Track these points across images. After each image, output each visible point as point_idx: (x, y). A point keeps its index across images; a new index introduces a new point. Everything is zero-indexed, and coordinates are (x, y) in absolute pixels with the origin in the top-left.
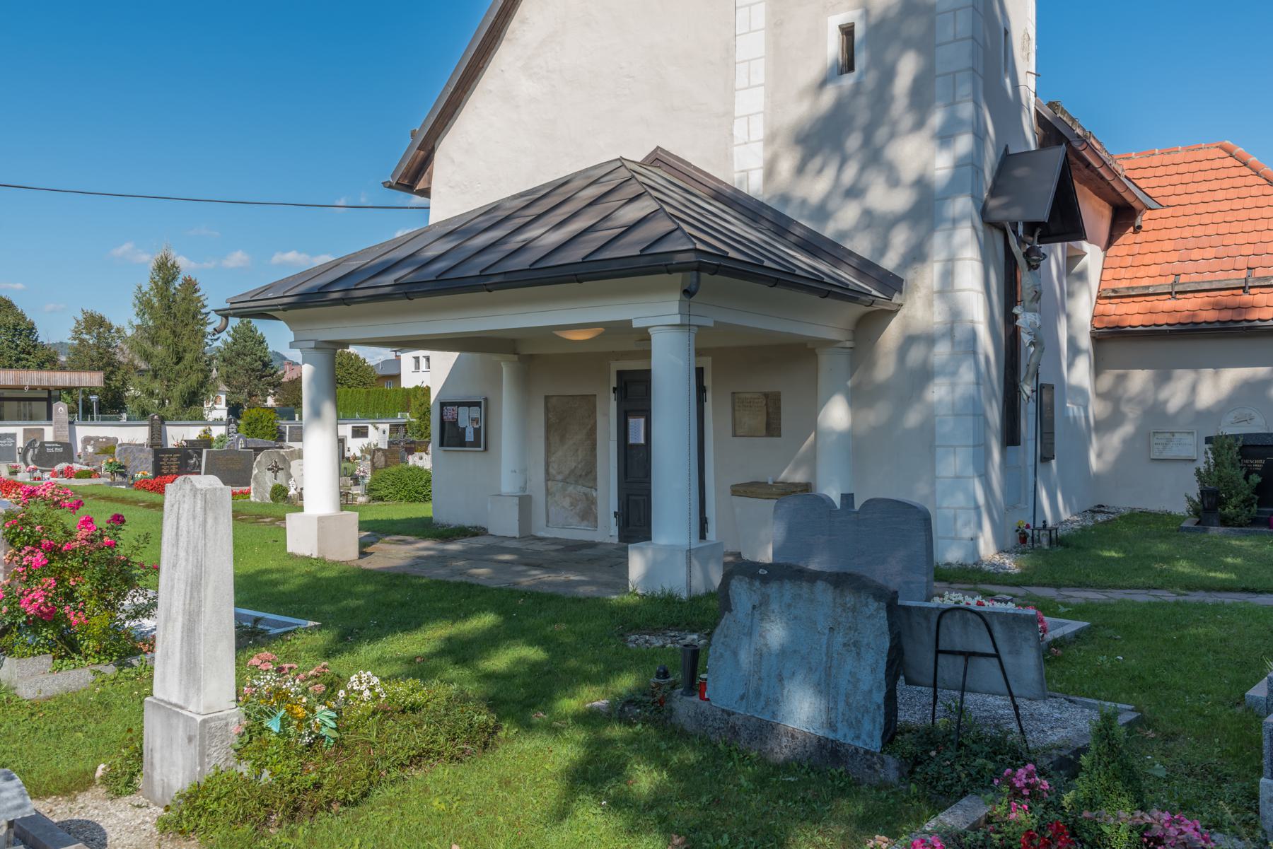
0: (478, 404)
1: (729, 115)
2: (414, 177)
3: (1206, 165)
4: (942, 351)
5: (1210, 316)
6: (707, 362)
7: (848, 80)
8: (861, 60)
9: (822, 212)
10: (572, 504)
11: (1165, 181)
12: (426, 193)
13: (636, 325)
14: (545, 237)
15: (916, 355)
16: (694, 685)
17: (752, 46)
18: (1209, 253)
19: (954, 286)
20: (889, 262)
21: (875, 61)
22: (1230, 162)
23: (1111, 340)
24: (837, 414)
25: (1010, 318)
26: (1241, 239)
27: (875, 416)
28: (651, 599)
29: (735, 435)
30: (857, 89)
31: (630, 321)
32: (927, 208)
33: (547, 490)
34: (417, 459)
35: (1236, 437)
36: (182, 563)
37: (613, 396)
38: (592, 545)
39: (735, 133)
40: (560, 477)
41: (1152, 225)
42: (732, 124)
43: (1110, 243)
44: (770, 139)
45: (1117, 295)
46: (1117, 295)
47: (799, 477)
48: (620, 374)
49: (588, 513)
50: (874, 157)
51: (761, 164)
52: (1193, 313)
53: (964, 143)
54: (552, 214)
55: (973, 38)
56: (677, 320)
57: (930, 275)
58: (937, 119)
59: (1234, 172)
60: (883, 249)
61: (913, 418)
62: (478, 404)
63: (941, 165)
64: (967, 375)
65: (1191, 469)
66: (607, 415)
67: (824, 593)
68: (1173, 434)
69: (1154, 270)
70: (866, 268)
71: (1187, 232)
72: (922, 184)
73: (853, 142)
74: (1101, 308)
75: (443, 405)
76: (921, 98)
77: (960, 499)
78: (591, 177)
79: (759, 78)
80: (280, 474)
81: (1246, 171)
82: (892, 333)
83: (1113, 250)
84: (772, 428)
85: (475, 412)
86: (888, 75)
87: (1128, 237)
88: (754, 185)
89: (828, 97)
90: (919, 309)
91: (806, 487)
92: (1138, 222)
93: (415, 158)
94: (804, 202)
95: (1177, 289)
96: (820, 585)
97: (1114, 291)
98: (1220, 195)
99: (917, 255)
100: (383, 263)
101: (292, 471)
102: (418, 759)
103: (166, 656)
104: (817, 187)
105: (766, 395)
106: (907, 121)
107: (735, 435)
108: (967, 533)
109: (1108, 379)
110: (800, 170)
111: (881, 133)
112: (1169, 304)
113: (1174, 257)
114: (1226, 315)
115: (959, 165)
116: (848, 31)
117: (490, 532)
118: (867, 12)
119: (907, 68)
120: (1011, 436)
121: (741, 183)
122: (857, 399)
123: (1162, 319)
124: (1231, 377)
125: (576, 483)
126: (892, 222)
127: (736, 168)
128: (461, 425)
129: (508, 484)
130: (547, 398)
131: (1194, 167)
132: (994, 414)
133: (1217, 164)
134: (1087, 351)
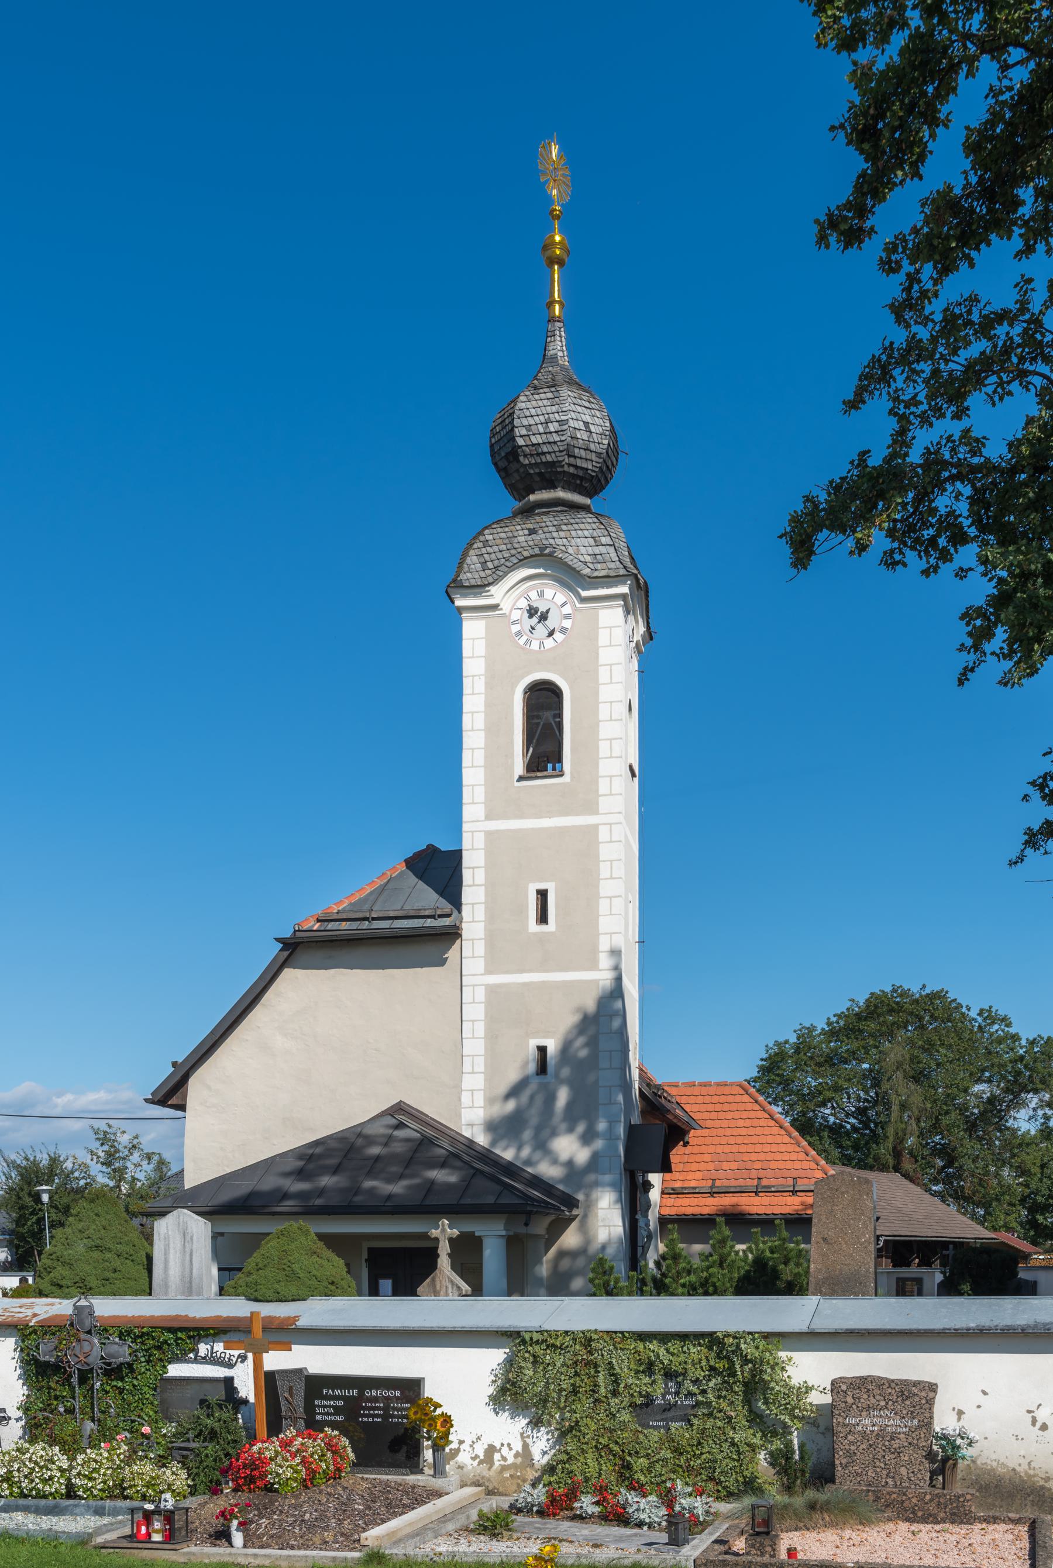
1: (458, 1089)
12: (182, 1108)
13: (477, 1234)
17: (474, 1046)
18: (734, 1165)
26: (754, 1157)
37: (364, 1264)
39: (463, 1100)
71: (719, 1149)
73: (527, 1134)
79: (481, 1068)
92: (686, 1139)
97: (673, 1189)
98: (741, 1123)
106: (563, 1126)
113: (711, 1166)
131: (723, 1099)
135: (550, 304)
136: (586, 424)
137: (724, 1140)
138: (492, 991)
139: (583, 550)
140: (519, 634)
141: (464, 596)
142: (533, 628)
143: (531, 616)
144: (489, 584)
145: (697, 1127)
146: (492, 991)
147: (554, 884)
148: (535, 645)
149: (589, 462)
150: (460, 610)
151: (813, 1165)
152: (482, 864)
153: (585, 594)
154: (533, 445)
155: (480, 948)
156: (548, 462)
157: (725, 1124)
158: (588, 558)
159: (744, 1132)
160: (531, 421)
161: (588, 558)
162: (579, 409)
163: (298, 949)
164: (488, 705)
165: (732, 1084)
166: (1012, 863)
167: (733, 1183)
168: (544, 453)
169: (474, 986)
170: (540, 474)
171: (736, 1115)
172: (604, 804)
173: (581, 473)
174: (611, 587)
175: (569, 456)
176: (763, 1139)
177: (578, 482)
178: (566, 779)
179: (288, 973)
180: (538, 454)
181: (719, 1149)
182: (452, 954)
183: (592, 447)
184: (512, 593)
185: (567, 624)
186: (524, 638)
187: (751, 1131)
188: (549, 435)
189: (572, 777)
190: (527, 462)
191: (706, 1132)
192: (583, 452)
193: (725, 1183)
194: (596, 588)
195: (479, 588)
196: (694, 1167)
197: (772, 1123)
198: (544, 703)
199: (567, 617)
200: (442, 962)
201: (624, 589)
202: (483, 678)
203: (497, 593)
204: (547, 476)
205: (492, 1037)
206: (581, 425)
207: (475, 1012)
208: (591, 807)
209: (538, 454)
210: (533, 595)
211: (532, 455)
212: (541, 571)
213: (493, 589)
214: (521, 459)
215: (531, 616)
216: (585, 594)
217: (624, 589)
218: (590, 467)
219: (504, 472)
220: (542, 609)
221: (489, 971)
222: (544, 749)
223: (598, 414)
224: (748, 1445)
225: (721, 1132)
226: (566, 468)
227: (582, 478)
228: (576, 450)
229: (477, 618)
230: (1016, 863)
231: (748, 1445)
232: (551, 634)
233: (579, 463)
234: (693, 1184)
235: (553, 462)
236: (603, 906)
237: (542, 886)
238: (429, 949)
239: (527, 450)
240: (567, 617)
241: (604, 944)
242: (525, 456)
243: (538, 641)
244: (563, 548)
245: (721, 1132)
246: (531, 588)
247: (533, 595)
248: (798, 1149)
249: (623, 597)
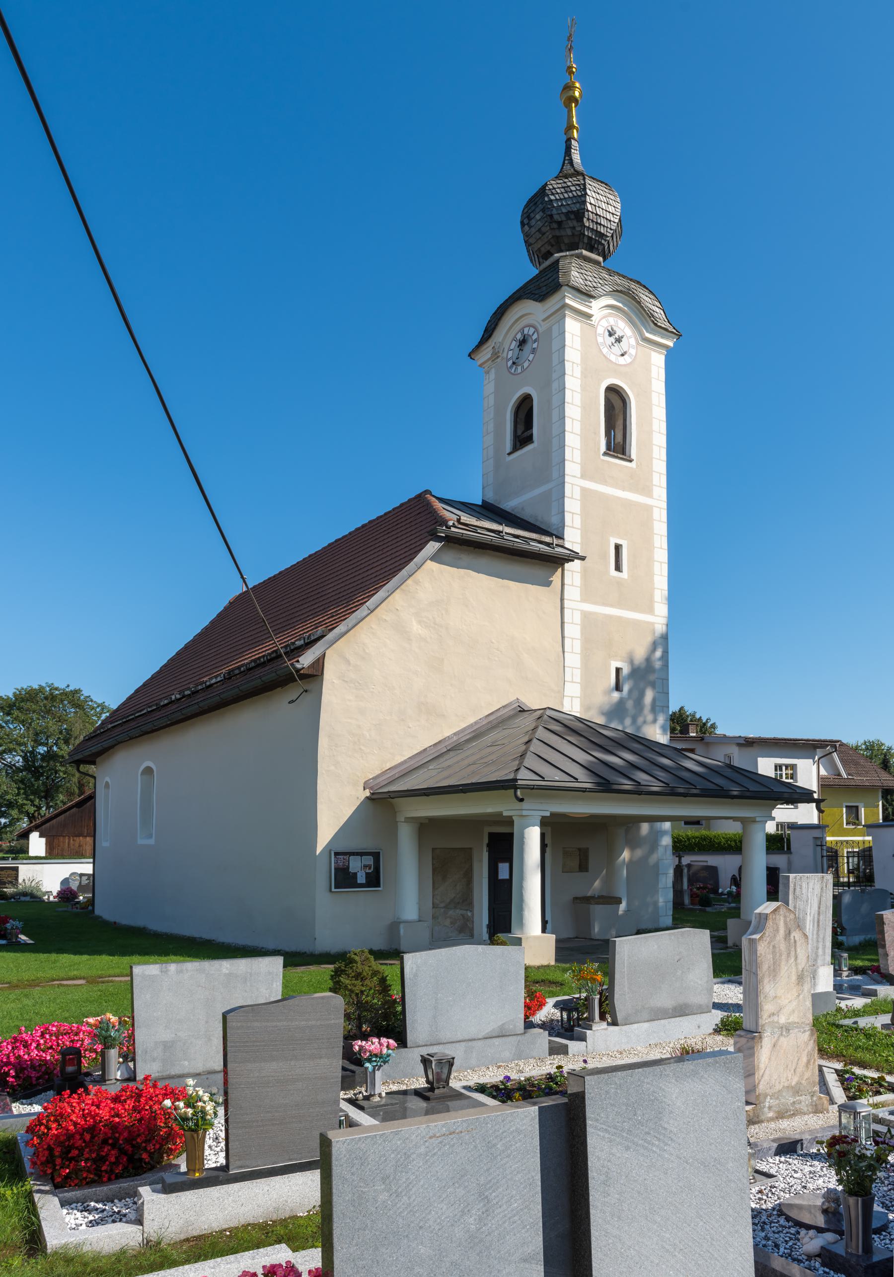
6: (548, 830)
10: (451, 923)
13: (505, 814)
24: (626, 855)
27: (639, 853)
37: (485, 849)
40: (442, 905)
48: (491, 835)
66: (481, 861)
84: (583, 867)
86: (642, 695)
88: (578, 715)
105: (580, 849)
111: (640, 720)
118: (631, 662)
125: (455, 908)
130: (433, 850)
150: (565, 306)
154: (597, 214)
168: (600, 224)
170: (590, 238)
180: (597, 223)
182: (556, 578)
194: (655, 335)
212: (620, 305)
214: (585, 220)
221: (583, 600)
224: (343, 1214)
231: (343, 1214)
235: (603, 234)
237: (619, 542)
238: (537, 571)
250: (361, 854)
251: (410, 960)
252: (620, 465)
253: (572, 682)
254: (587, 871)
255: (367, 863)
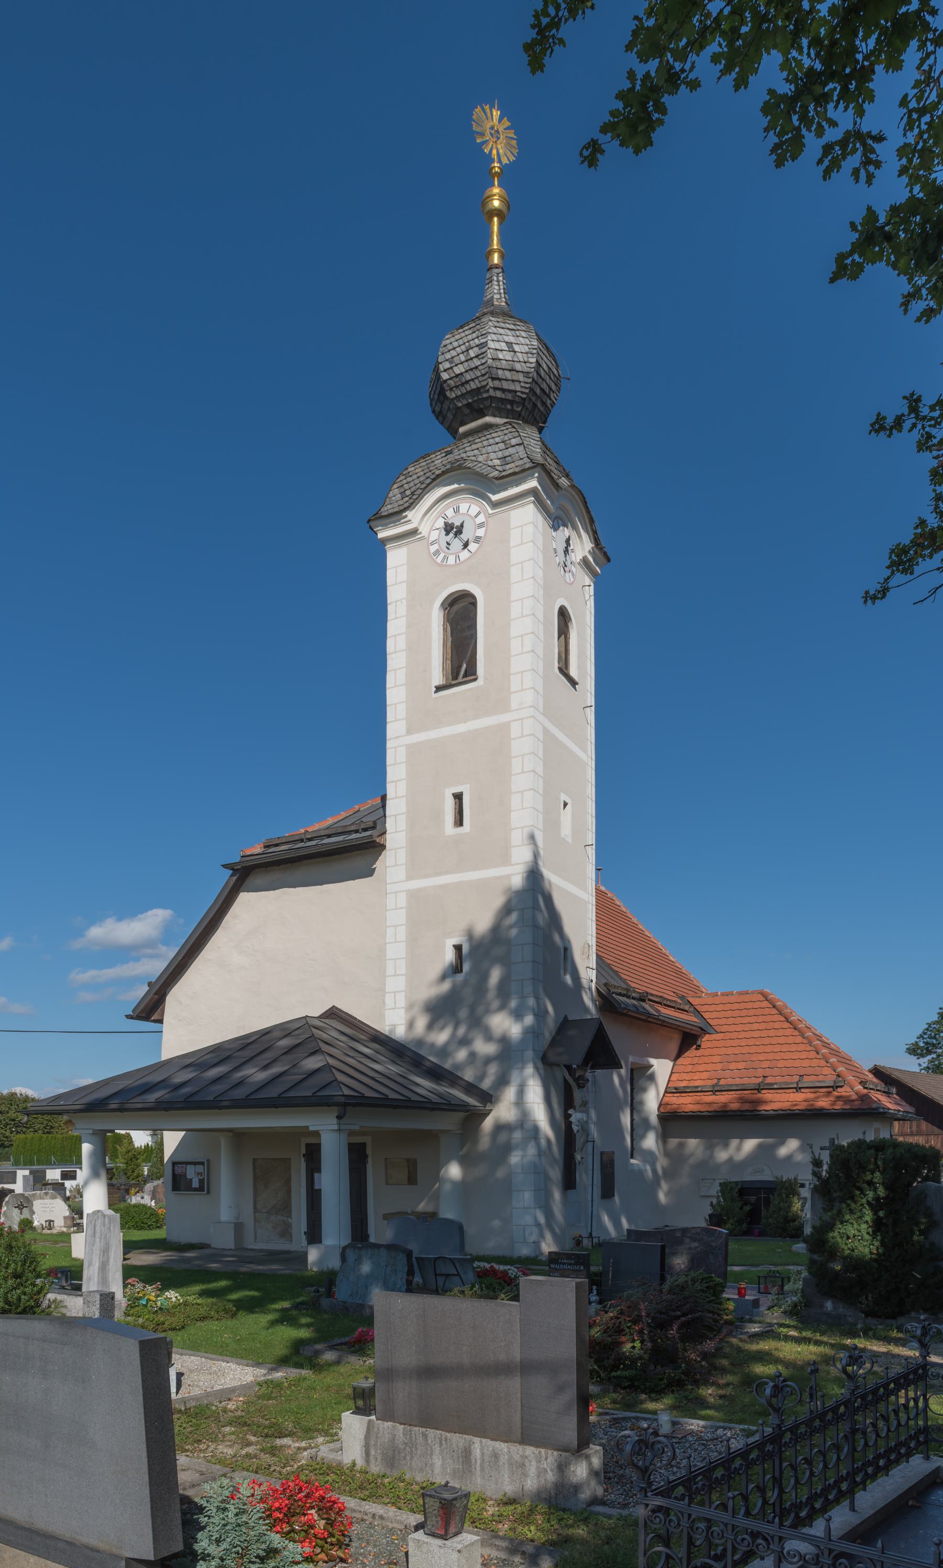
0: (202, 1163)
1: (382, 991)
2: (151, 1009)
3: (750, 1005)
4: (517, 1135)
5: (735, 1106)
7: (460, 977)
8: (466, 967)
9: (444, 1051)
11: (721, 1014)
12: (160, 1021)
13: (311, 1129)
14: (255, 1075)
15: (503, 1137)
16: (330, 1294)
17: (396, 950)
18: (741, 1065)
19: (527, 1100)
20: (486, 1084)
21: (475, 968)
22: (766, 1004)
23: (671, 1121)
24: (454, 1171)
25: (567, 1116)
26: (762, 1057)
28: (321, 1273)
29: (387, 1184)
30: (466, 982)
31: (308, 1127)
32: (508, 1054)
33: (255, 1218)
34: (139, 1198)
35: (737, 1183)
36: (98, 1243)
37: (303, 1159)
38: (288, 1252)
39: (386, 1001)
41: (709, 1044)
42: (384, 996)
43: (678, 1056)
44: (410, 1007)
45: (678, 1091)
46: (678, 1091)
47: (430, 1209)
48: (308, 1145)
49: (286, 1232)
50: (477, 1023)
51: (404, 1022)
52: (725, 1105)
53: (529, 1020)
54: (259, 1058)
55: (534, 961)
56: (336, 1127)
57: (510, 1094)
58: (513, 1004)
59: (767, 1011)
60: (482, 1077)
61: (500, 1173)
62: (202, 1163)
63: (515, 1030)
64: (531, 1151)
65: (708, 1202)
67: (383, 1252)
68: (714, 1180)
69: (705, 1075)
70: (471, 1088)
71: (730, 1051)
72: (504, 1040)
73: (463, 1013)
74: (666, 1099)
75: (174, 1164)
76: (504, 991)
77: (529, 1220)
78: (285, 1029)
79: (402, 970)
80: (25, 1210)
81: (774, 1011)
82: (488, 1123)
83: (680, 1061)
84: (412, 1180)
85: (200, 1168)
86: (485, 977)
87: (692, 1052)
89: (446, 986)
90: (504, 1110)
91: (434, 1215)
92: (699, 1043)
93: (152, 999)
94: (432, 1045)
95: (716, 1089)
96: (382, 1249)
97: (676, 1088)
98: (756, 1026)
99: (502, 1081)
100: (146, 1084)
101: (34, 1208)
102: (203, 1319)
103: (89, 1279)
104: (442, 1037)
105: (408, 1160)
106: (496, 1004)
107: (387, 1184)
108: (533, 1238)
109: (673, 1142)
110: (430, 1027)
111: (480, 1009)
112: (710, 1098)
113: (719, 1067)
114: (746, 1107)
115: (527, 1032)
116: (458, 948)
117: (213, 1246)
119: (495, 976)
120: (569, 1183)
121: (391, 1031)
122: (464, 1162)
123: (704, 1108)
124: (750, 1144)
126: (488, 1060)
127: (387, 1023)
128: (189, 1177)
129: (226, 1214)
130: (255, 1160)
131: (742, 1006)
132: (556, 1174)
133: (757, 1005)
134: (654, 1128)
135: (491, 252)
136: (509, 344)
137: (736, 1043)
138: (413, 896)
139: (493, 456)
140: (437, 553)
141: (386, 526)
142: (448, 544)
143: (447, 534)
144: (405, 509)
145: (713, 1031)
146: (413, 896)
147: (468, 786)
148: (451, 560)
149: (517, 384)
150: (384, 542)
151: (823, 1063)
152: (404, 776)
153: (495, 498)
154: (457, 376)
155: (402, 857)
156: (473, 390)
157: (739, 1028)
158: (497, 462)
159: (756, 1034)
160: (453, 353)
161: (497, 462)
162: (502, 331)
163: (246, 875)
164: (409, 626)
165: (753, 992)
166: (871, 598)
167: (738, 1081)
168: (467, 382)
169: (396, 893)
170: (468, 405)
171: (753, 1019)
172: (515, 701)
173: (509, 397)
174: (520, 484)
175: (493, 379)
176: (774, 1041)
177: (509, 407)
178: (480, 682)
179: (244, 898)
180: (463, 384)
181: (730, 1051)
183: (518, 367)
184: (426, 517)
185: (480, 532)
186: (442, 555)
187: (764, 1034)
188: (470, 362)
189: (486, 679)
190: (453, 395)
191: (720, 1036)
192: (507, 373)
193: (730, 1081)
194: (506, 489)
195: (397, 515)
196: (702, 1068)
197: (787, 1025)
198: (461, 613)
199: (481, 525)
200: (370, 873)
201: (533, 483)
202: (404, 601)
203: (414, 517)
204: (475, 406)
205: (413, 941)
206: (504, 346)
207: (397, 916)
208: (503, 705)
209: (463, 384)
210: (450, 513)
211: (457, 387)
212: (456, 486)
213: (410, 514)
214: (448, 393)
215: (447, 534)
216: (495, 498)
217: (533, 483)
218: (518, 389)
219: (440, 415)
220: (457, 523)
221: (409, 878)
222: (461, 661)
223: (523, 334)
225: (734, 1035)
226: (492, 393)
227: (512, 402)
228: (500, 372)
229: (399, 546)
230: (874, 598)
232: (466, 545)
233: (505, 385)
234: (697, 1083)
235: (478, 389)
236: (515, 801)
237: (457, 790)
239: (451, 383)
240: (481, 525)
241: (518, 838)
242: (451, 389)
243: (457, 555)
244: (473, 458)
245: (734, 1035)
246: (447, 507)
247: (450, 513)
248: (809, 1048)
249: (533, 492)
250: (195, 1163)
251: (671, 1064)
252: (470, 690)
253: (395, 975)
254: (416, 1184)
255: (200, 1171)
